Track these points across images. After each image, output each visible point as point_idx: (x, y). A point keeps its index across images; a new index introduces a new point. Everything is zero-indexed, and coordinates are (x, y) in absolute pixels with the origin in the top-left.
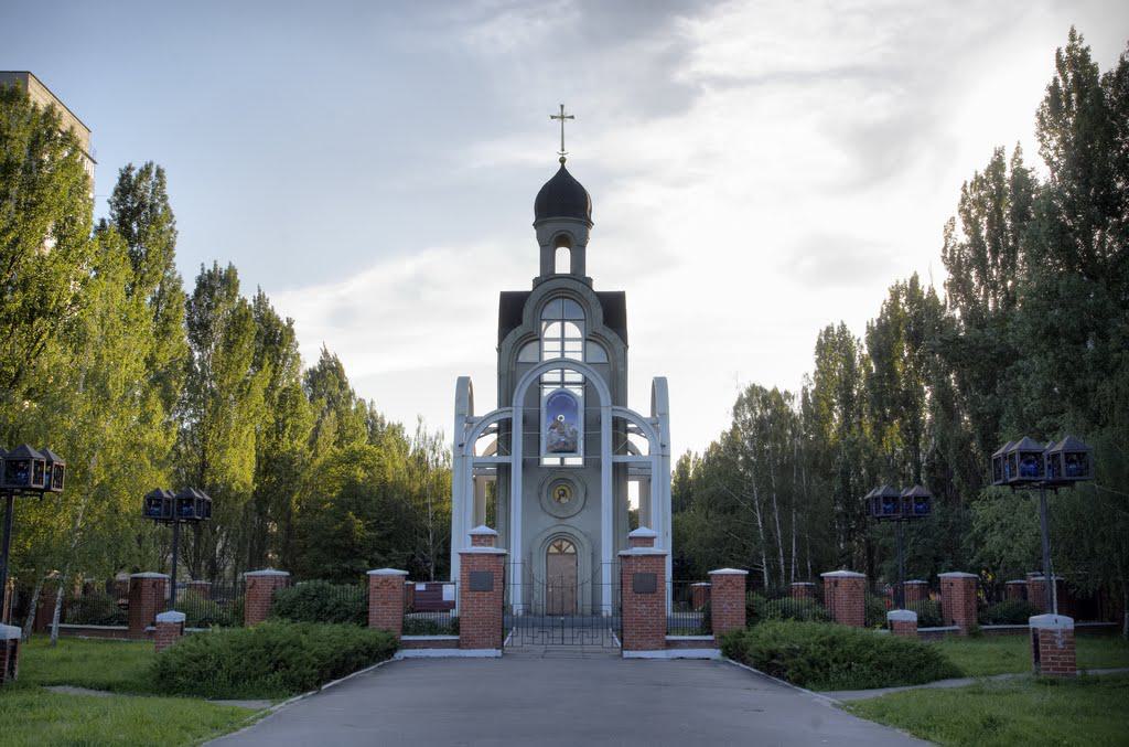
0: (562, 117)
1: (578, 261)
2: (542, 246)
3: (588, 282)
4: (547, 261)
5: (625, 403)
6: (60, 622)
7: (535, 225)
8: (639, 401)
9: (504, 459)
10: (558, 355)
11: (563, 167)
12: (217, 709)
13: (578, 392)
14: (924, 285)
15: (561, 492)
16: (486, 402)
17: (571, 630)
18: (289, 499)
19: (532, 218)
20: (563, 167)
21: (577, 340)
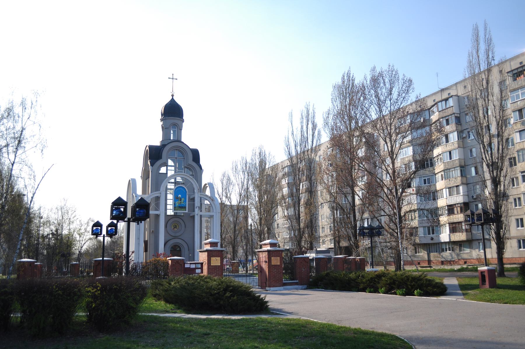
0: (173, 79)
11: (173, 98)
20: (173, 98)
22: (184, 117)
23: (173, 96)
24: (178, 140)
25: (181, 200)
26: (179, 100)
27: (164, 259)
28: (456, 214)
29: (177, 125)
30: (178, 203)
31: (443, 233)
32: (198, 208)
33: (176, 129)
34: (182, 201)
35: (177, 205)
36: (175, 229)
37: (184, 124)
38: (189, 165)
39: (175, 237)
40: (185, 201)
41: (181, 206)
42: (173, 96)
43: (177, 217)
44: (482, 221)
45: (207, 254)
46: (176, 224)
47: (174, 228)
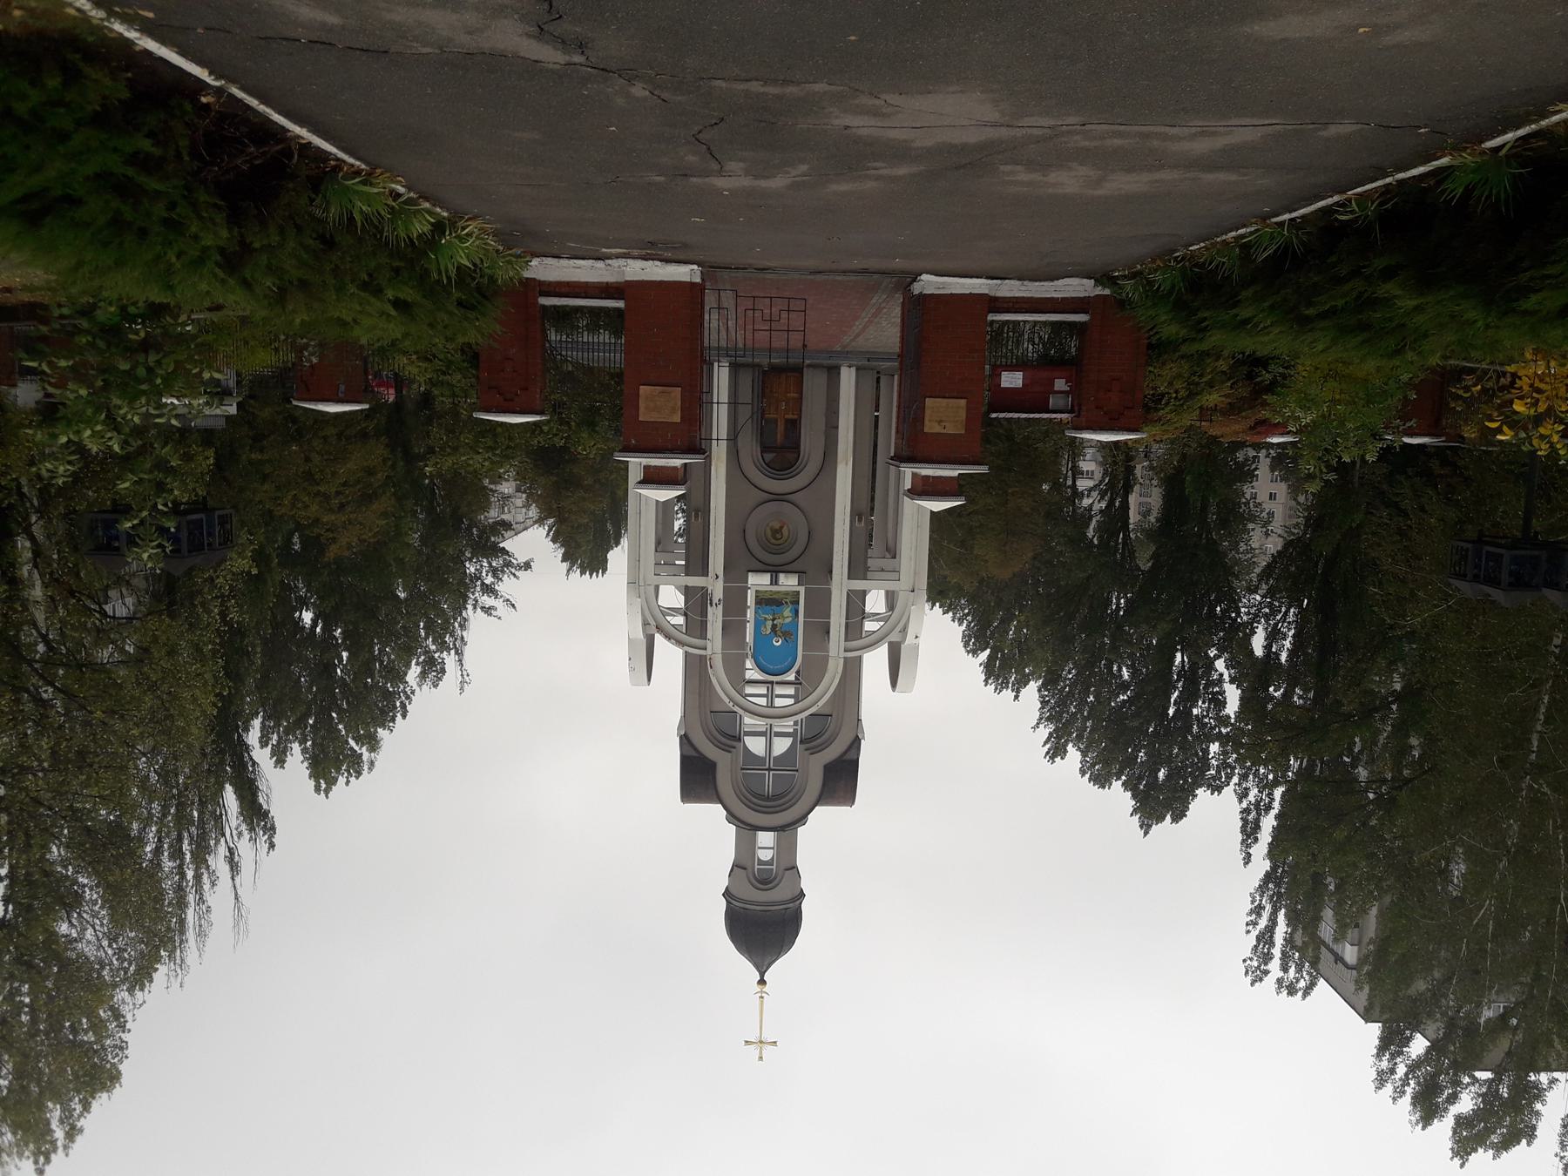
0: (761, 1042)
1: (745, 847)
2: (793, 868)
3: (732, 817)
4: (787, 848)
5: (688, 658)
6: (204, 549)
7: (802, 895)
8: (670, 657)
9: (858, 585)
10: (704, 401)
11: (762, 974)
12: (1144, 296)
13: (752, 673)
14: (387, 732)
15: (778, 536)
16: (875, 663)
17: (774, 345)
18: (174, 396)
19: (806, 906)
20: (762, 974)
21: (760, 848)
22: (722, 905)
23: (762, 982)
24: (746, 829)
25: (774, 627)
26: (745, 968)
27: (348, 466)
28: (1510, 373)
29: (754, 881)
30: (784, 618)
31: (802, 720)
32: (715, 600)
33: (757, 867)
34: (769, 623)
35: (787, 612)
36: (777, 525)
37: (725, 882)
38: (727, 749)
39: (779, 497)
40: (758, 624)
41: (774, 608)
42: (762, 982)
43: (771, 568)
44: (219, 516)
45: (963, 414)
46: (773, 541)
47: (781, 527)
